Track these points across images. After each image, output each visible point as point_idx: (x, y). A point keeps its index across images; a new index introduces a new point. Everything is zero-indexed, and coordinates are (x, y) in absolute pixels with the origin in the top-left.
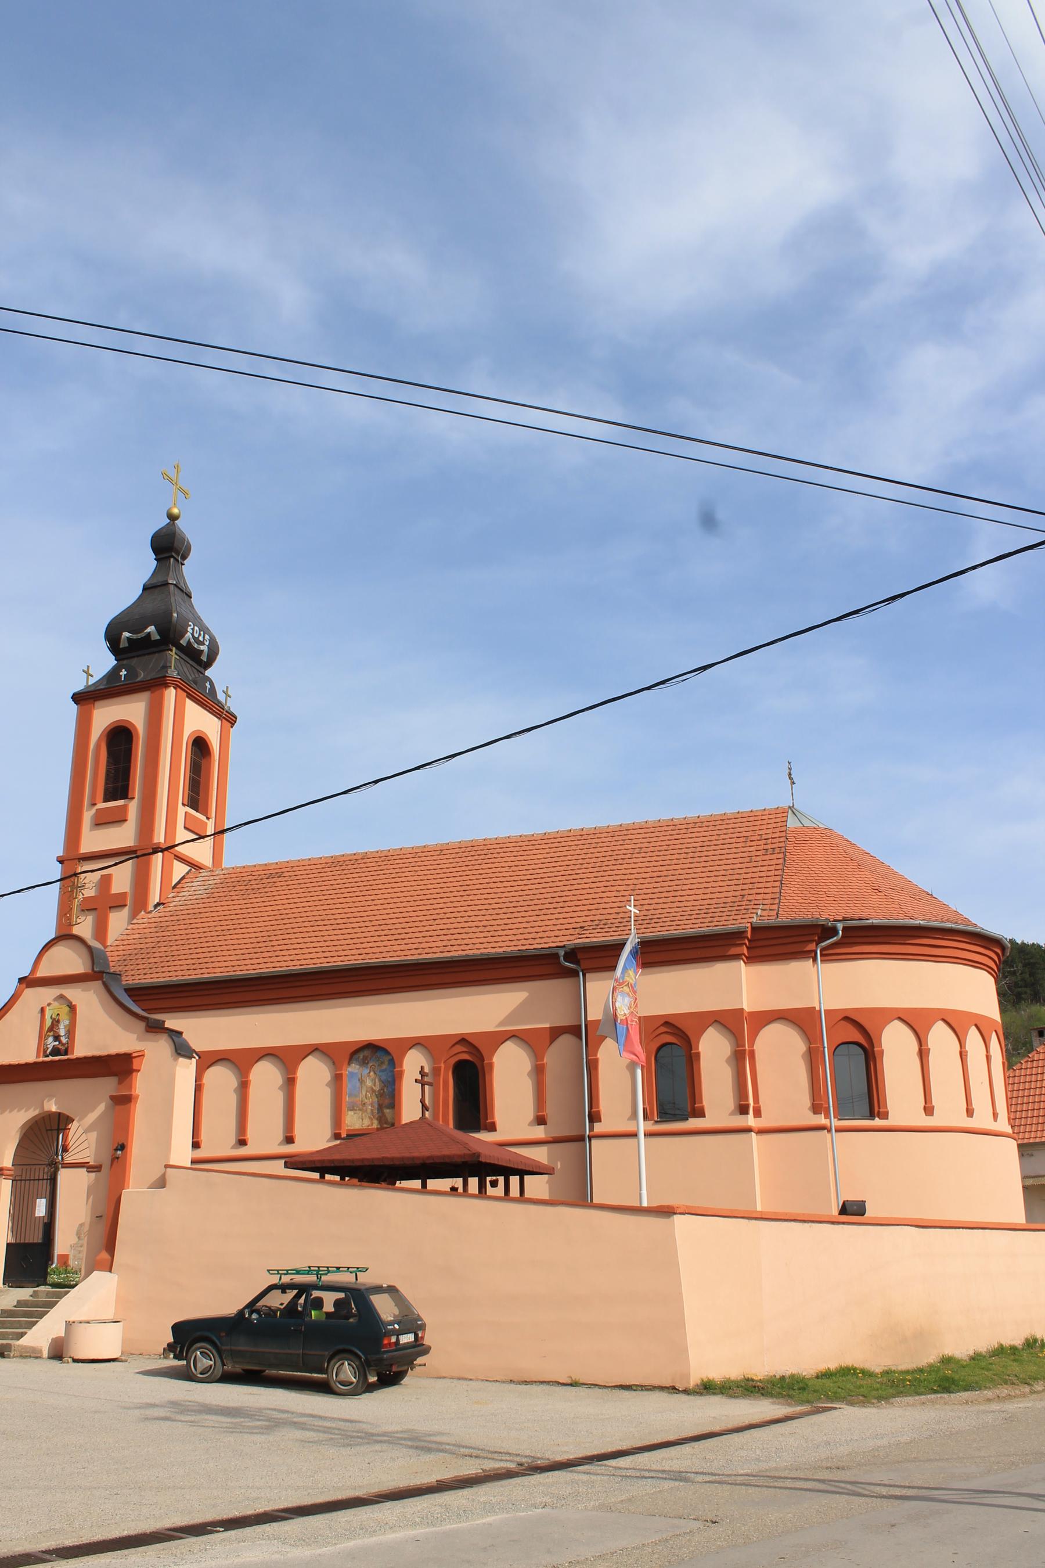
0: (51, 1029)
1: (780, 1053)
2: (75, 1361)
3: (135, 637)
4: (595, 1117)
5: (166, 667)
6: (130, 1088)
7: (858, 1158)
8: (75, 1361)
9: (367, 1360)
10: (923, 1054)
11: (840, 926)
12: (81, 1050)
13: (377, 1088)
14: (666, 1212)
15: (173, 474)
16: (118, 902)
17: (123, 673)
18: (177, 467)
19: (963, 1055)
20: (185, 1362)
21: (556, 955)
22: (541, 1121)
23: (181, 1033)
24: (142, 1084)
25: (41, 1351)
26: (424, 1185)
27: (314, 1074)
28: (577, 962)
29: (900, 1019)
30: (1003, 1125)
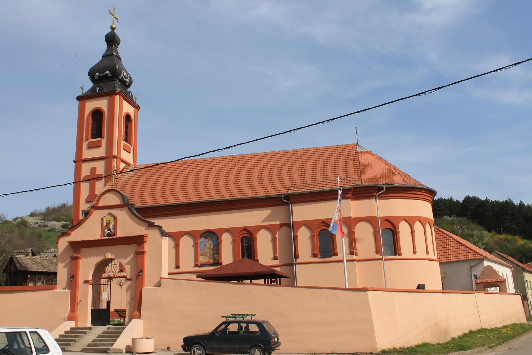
0: (106, 226)
1: (364, 233)
2: (138, 353)
3: (101, 75)
4: (297, 257)
5: (115, 87)
6: (143, 248)
7: (392, 268)
8: (138, 353)
9: (265, 348)
10: (412, 232)
11: (385, 187)
12: (120, 234)
13: (212, 246)
14: (365, 290)
15: (112, 11)
16: (99, 178)
17: (98, 89)
18: (114, 9)
19: (425, 233)
20: (189, 352)
21: (281, 197)
22: (275, 258)
23: (162, 227)
24: (147, 247)
25: (122, 350)
26: (251, 282)
27: (186, 242)
28: (289, 200)
29: (405, 220)
30: (436, 258)
